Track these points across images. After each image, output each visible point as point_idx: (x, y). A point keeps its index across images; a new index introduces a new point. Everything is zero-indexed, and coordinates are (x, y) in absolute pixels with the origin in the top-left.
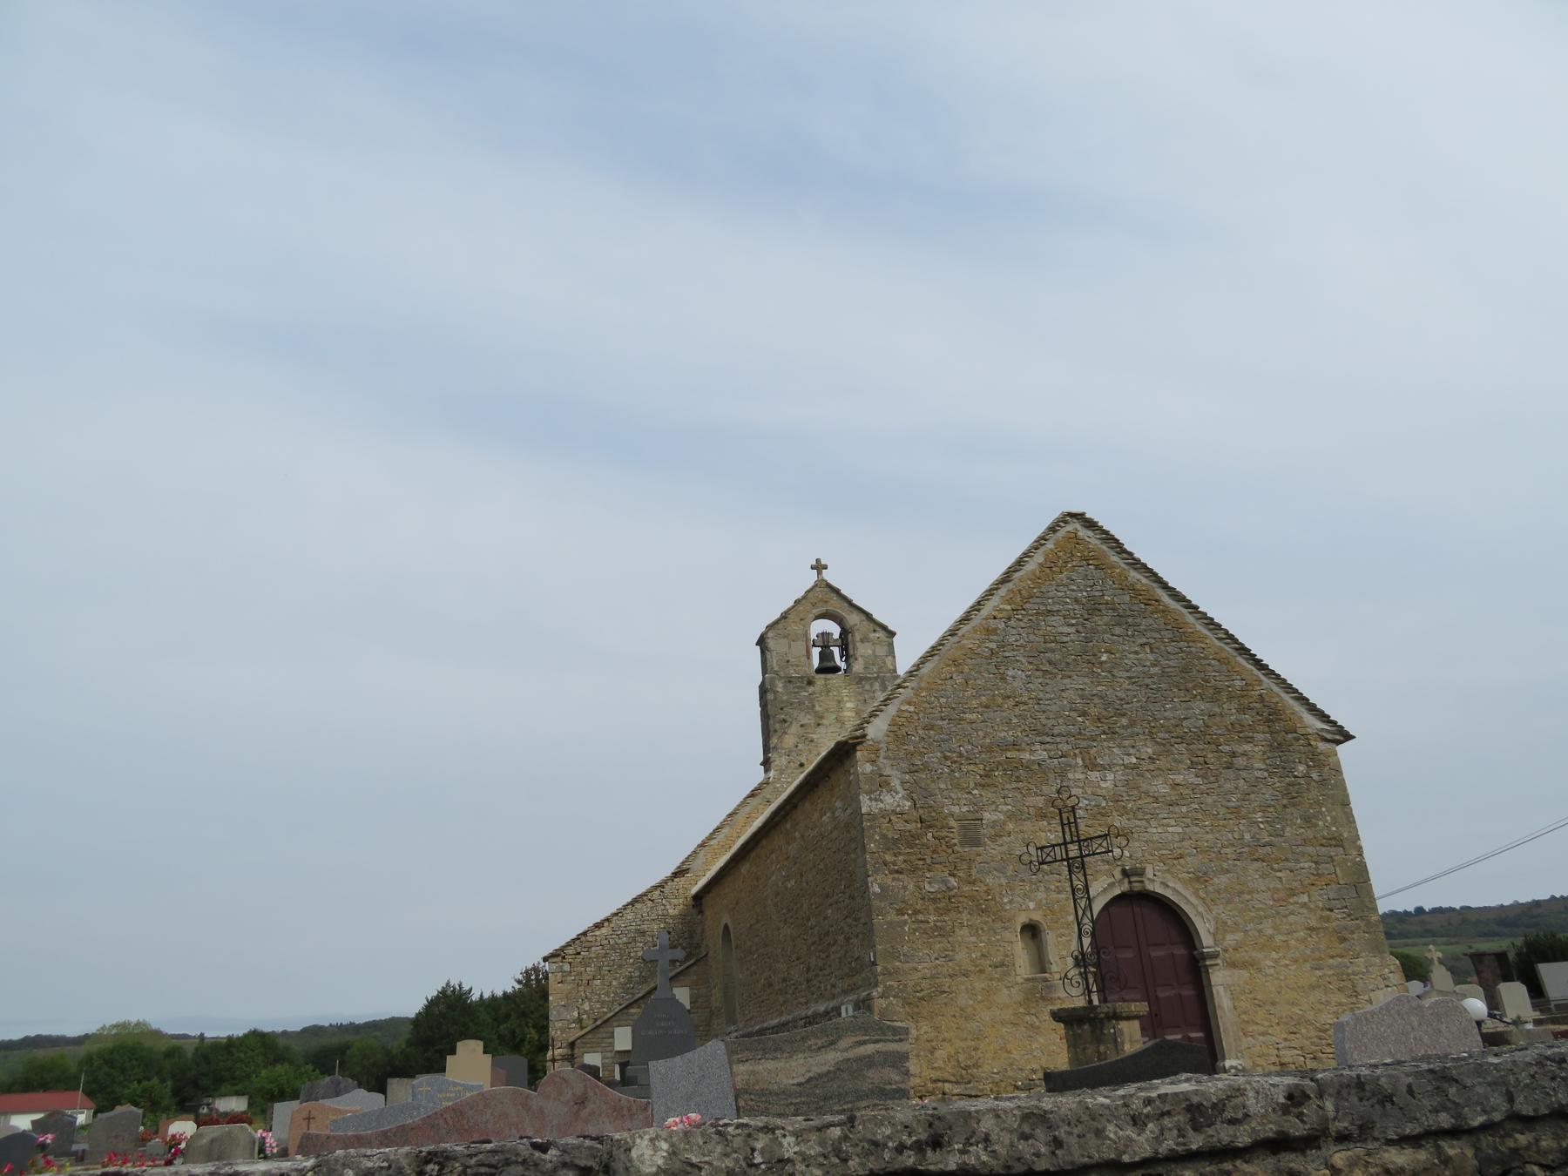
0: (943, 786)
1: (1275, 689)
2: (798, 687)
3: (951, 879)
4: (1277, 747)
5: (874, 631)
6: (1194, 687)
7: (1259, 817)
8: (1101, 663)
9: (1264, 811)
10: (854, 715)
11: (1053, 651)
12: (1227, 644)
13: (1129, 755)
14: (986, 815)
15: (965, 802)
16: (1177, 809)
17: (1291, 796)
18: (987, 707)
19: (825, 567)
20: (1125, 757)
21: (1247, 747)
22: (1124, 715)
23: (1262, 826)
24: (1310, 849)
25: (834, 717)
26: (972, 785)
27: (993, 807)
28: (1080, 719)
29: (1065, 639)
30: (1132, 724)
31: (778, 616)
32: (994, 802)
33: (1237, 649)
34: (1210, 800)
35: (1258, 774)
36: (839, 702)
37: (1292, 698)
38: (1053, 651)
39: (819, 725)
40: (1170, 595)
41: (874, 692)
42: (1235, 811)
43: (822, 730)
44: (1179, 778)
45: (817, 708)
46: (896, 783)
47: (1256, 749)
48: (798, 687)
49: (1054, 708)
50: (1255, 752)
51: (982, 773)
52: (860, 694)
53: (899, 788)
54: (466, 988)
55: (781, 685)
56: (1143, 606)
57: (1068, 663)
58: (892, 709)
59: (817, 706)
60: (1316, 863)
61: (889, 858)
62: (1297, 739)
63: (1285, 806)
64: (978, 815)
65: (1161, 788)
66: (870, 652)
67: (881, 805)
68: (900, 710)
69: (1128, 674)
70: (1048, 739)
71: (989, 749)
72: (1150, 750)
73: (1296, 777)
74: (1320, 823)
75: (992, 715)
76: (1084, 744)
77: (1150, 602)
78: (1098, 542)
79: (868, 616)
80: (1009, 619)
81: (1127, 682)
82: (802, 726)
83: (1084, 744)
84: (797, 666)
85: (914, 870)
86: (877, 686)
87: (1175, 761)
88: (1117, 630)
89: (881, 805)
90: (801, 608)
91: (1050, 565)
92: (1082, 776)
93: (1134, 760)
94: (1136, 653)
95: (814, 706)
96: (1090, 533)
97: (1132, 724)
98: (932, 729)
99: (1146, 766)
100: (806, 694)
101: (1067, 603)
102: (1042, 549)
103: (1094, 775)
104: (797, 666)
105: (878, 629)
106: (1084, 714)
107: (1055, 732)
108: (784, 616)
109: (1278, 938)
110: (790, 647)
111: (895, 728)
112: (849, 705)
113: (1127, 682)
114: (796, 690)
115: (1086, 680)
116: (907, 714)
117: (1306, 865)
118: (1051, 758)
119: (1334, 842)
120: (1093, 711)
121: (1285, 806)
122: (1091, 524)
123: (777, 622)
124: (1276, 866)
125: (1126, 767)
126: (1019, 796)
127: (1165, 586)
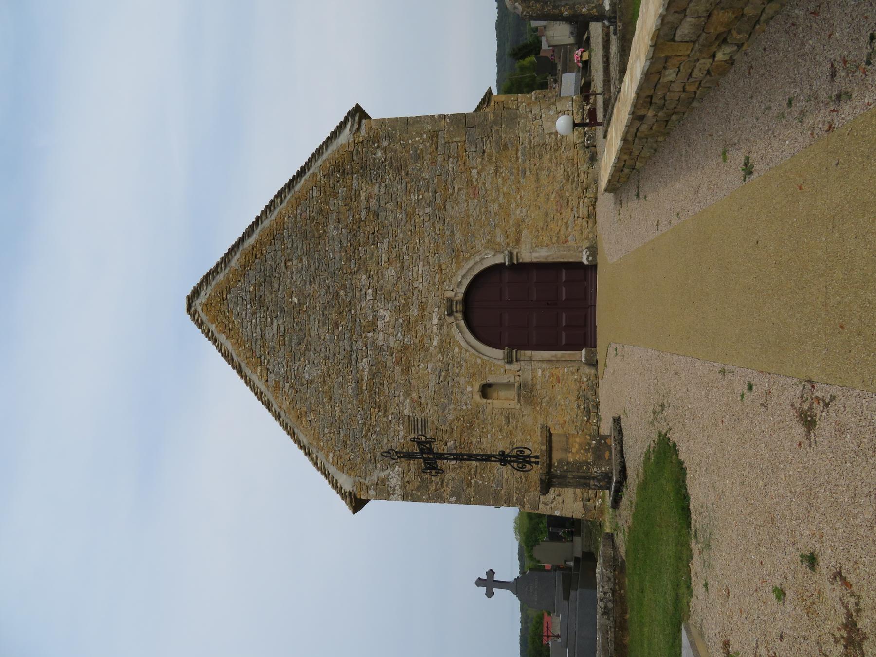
74: (421, 146)
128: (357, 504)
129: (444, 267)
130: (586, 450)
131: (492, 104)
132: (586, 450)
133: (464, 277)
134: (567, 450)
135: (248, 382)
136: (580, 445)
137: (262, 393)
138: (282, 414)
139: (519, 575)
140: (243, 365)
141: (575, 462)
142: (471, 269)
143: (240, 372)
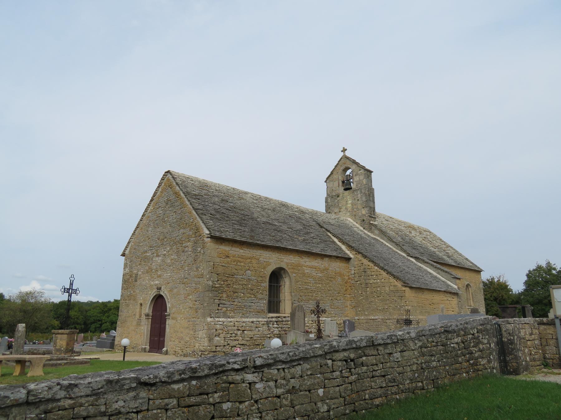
2: (335, 199)
5: (360, 170)
9: (188, 266)
10: (351, 205)
19: (346, 150)
31: (330, 173)
36: (347, 201)
39: (340, 211)
41: (358, 195)
43: (341, 213)
45: (340, 205)
48: (335, 199)
54: (507, 284)
55: (329, 199)
66: (358, 179)
72: (168, 249)
74: (200, 270)
82: (335, 213)
84: (335, 191)
86: (359, 192)
90: (337, 168)
100: (337, 201)
102: (161, 186)
104: (335, 191)
105: (361, 169)
108: (332, 173)
109: (183, 310)
121: (193, 264)
123: (329, 176)
128: (123, 255)
129: (169, 285)
130: (60, 346)
131: (404, 289)
132: (60, 346)
133: (165, 294)
134: (61, 339)
135: (149, 205)
136: (62, 344)
137: (147, 211)
138: (142, 221)
139: (524, 287)
140: (153, 201)
141: (57, 342)
142: (167, 296)
143: (151, 201)
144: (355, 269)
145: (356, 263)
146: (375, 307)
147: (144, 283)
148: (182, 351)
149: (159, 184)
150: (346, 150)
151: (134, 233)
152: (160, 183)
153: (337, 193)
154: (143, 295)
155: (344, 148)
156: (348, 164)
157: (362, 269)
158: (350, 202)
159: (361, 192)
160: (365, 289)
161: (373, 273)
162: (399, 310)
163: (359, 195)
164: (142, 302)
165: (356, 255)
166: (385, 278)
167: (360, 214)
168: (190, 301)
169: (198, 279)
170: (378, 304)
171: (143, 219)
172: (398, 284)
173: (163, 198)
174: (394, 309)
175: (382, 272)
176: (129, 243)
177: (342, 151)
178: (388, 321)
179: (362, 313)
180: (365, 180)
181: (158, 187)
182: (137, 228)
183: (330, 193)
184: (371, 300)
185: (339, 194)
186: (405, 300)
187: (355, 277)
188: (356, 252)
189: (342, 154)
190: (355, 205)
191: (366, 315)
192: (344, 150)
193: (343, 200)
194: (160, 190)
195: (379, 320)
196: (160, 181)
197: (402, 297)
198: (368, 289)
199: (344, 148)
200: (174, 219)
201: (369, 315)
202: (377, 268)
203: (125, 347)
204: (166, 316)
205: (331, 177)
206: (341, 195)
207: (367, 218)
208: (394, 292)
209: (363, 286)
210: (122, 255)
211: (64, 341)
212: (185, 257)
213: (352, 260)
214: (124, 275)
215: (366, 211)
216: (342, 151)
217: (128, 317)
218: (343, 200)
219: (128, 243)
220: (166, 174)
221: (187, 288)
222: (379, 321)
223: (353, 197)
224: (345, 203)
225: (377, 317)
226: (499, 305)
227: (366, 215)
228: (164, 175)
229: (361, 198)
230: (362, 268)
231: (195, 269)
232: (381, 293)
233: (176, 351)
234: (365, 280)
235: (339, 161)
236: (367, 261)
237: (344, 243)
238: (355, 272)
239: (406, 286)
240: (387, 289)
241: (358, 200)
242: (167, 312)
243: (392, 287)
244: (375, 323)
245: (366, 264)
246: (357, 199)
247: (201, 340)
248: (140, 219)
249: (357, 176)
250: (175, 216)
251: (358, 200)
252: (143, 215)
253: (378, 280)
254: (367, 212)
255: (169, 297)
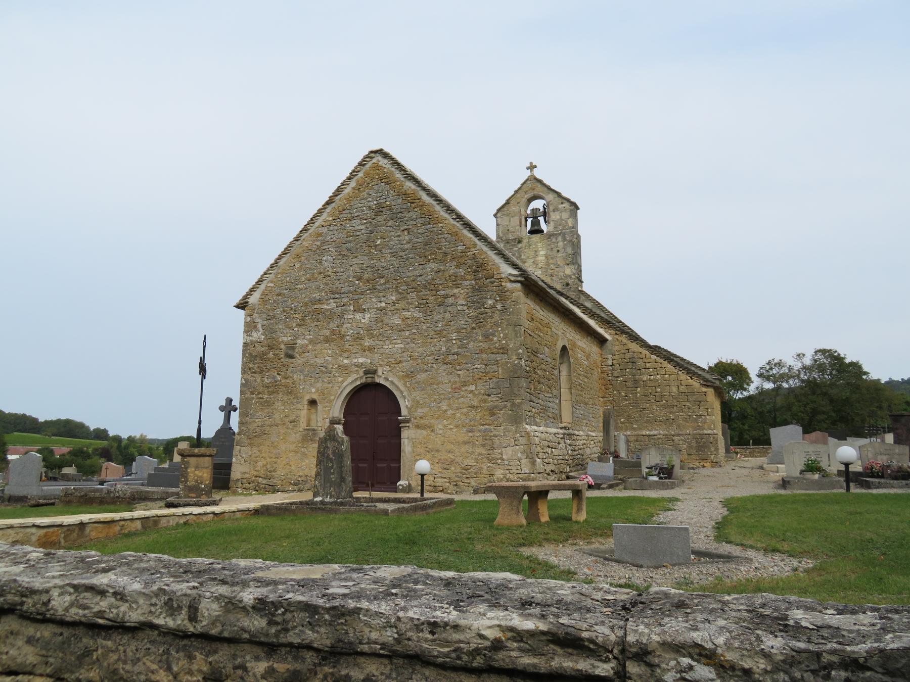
0: (280, 327)
1: (485, 249)
2: (512, 245)
3: (278, 376)
4: (478, 290)
5: (562, 203)
6: (431, 255)
7: (454, 336)
8: (376, 246)
10: (544, 258)
11: (350, 242)
12: (458, 222)
13: (381, 302)
14: (299, 341)
15: (290, 335)
16: (403, 333)
17: (479, 322)
18: (309, 280)
19: (535, 167)
20: (378, 303)
21: (456, 291)
22: (383, 277)
23: (454, 342)
24: (484, 356)
25: (532, 261)
26: (294, 325)
27: (303, 337)
28: (357, 282)
29: (358, 233)
30: (387, 282)
32: (304, 334)
33: (463, 224)
34: (424, 327)
35: (460, 308)
36: (536, 251)
37: (495, 253)
38: (350, 242)
40: (428, 194)
42: (439, 333)
44: (408, 314)
45: (523, 257)
46: (259, 326)
47: (462, 291)
48: (512, 245)
49: (345, 277)
50: (460, 295)
51: (300, 318)
52: (549, 245)
53: (261, 329)
56: (409, 204)
57: (357, 249)
58: (262, 287)
59: (523, 255)
60: (486, 365)
61: (251, 365)
62: (492, 283)
63: (473, 328)
64: (295, 342)
65: (397, 321)
66: (558, 217)
67: (251, 338)
68: (267, 287)
69: (391, 251)
70: (337, 296)
71: (306, 305)
72: (394, 298)
73: (486, 308)
74: (495, 339)
75: (310, 285)
76: (356, 297)
77: (415, 201)
78: (390, 166)
79: (559, 194)
80: (330, 226)
81: (389, 256)
83: (356, 297)
84: (514, 232)
85: (261, 371)
86: (560, 238)
87: (408, 303)
88: (390, 223)
89: (251, 338)
90: (518, 195)
91: (358, 189)
92: (352, 317)
93: (383, 304)
94: (399, 236)
95: (521, 256)
96: (386, 161)
97: (387, 282)
98: (280, 295)
99: (390, 308)
100: (516, 249)
101: (364, 210)
102: (356, 178)
103: (359, 316)
104: (514, 232)
105: (565, 201)
106: (360, 279)
107: (342, 291)
108: (508, 202)
110: (510, 221)
111: (263, 297)
112: (542, 253)
113: (389, 256)
114: (511, 247)
115: (365, 257)
116: (270, 288)
117: (479, 366)
118: (337, 307)
119: (501, 351)
120: (366, 276)
121: (473, 328)
122: (386, 155)
123: (503, 207)
124: (458, 367)
125: (378, 309)
126: (317, 330)
127: (425, 189)
129: (400, 365)
130: (197, 481)
131: (704, 389)
133: (392, 383)
134: (197, 467)
135: (320, 212)
137: (313, 223)
140: (333, 205)
141: (187, 473)
143: (328, 203)
144: (614, 357)
145: (616, 348)
146: (650, 417)
147: (319, 361)
148: (456, 485)
149: (351, 174)
150: (535, 167)
151: (276, 262)
152: (353, 171)
153: (516, 237)
154: (319, 385)
155: (531, 163)
156: (539, 190)
157: (627, 357)
158: (542, 253)
159: (564, 239)
160: (633, 389)
161: (648, 365)
162: (696, 421)
163: (561, 244)
164: (315, 397)
165: (617, 336)
166: (670, 373)
167: (561, 274)
168: (471, 395)
169: (493, 356)
170: (658, 413)
171: (302, 238)
172: (695, 383)
173: (363, 201)
174: (685, 420)
175: (665, 363)
176: (259, 282)
177: (528, 168)
178: (676, 438)
179: (627, 427)
180: (571, 219)
181: (349, 178)
182: (285, 253)
183: (504, 234)
184: (645, 407)
185: (522, 238)
186: (706, 407)
187: (613, 370)
188: (617, 332)
189: (528, 173)
190: (552, 258)
191: (635, 429)
192: (532, 167)
193: (530, 248)
194: (353, 184)
195: (659, 436)
196: (356, 168)
197: (700, 402)
198: (639, 389)
199: (531, 163)
200: (405, 242)
201: (639, 429)
202: (656, 357)
203: (423, 476)
204: (400, 422)
205: (505, 209)
206: (525, 241)
207: (573, 282)
208: (688, 394)
209: (629, 384)
210: (238, 307)
211: (205, 470)
212: (448, 316)
213: (608, 344)
214: (245, 345)
215: (574, 271)
216: (528, 168)
217: (270, 426)
218: (530, 248)
219: (259, 281)
220: (372, 155)
221: (459, 372)
222: (659, 438)
223: (549, 245)
224: (532, 253)
225: (655, 432)
226: (52, 450)
227: (573, 277)
228: (367, 157)
229: (564, 248)
230: (628, 356)
231: (481, 338)
232: (662, 396)
233: (437, 484)
234: (634, 375)
235: (522, 185)
236: (638, 346)
237: (593, 315)
238: (615, 362)
239: (708, 386)
240: (674, 389)
241: (558, 251)
242: (401, 416)
243: (683, 387)
244: (652, 441)
245: (636, 350)
246: (555, 250)
247: (511, 463)
248: (295, 236)
249: (557, 213)
250: (407, 238)
251: (558, 251)
252: (305, 230)
253: (658, 376)
254: (574, 271)
255: (402, 388)
